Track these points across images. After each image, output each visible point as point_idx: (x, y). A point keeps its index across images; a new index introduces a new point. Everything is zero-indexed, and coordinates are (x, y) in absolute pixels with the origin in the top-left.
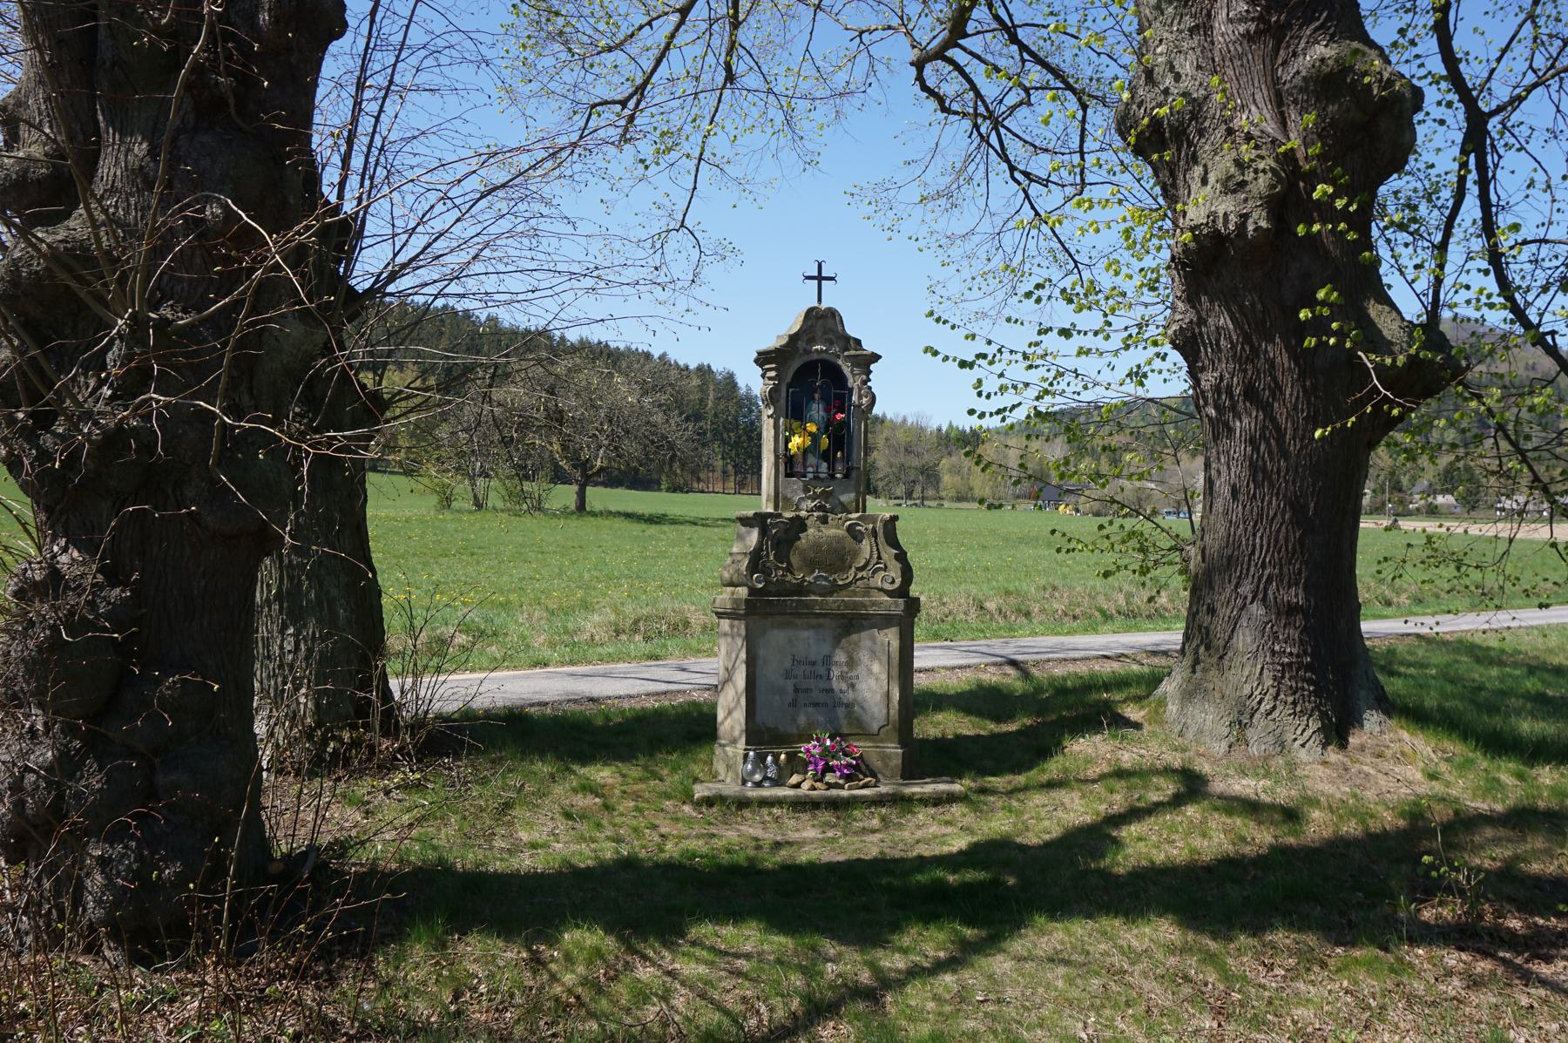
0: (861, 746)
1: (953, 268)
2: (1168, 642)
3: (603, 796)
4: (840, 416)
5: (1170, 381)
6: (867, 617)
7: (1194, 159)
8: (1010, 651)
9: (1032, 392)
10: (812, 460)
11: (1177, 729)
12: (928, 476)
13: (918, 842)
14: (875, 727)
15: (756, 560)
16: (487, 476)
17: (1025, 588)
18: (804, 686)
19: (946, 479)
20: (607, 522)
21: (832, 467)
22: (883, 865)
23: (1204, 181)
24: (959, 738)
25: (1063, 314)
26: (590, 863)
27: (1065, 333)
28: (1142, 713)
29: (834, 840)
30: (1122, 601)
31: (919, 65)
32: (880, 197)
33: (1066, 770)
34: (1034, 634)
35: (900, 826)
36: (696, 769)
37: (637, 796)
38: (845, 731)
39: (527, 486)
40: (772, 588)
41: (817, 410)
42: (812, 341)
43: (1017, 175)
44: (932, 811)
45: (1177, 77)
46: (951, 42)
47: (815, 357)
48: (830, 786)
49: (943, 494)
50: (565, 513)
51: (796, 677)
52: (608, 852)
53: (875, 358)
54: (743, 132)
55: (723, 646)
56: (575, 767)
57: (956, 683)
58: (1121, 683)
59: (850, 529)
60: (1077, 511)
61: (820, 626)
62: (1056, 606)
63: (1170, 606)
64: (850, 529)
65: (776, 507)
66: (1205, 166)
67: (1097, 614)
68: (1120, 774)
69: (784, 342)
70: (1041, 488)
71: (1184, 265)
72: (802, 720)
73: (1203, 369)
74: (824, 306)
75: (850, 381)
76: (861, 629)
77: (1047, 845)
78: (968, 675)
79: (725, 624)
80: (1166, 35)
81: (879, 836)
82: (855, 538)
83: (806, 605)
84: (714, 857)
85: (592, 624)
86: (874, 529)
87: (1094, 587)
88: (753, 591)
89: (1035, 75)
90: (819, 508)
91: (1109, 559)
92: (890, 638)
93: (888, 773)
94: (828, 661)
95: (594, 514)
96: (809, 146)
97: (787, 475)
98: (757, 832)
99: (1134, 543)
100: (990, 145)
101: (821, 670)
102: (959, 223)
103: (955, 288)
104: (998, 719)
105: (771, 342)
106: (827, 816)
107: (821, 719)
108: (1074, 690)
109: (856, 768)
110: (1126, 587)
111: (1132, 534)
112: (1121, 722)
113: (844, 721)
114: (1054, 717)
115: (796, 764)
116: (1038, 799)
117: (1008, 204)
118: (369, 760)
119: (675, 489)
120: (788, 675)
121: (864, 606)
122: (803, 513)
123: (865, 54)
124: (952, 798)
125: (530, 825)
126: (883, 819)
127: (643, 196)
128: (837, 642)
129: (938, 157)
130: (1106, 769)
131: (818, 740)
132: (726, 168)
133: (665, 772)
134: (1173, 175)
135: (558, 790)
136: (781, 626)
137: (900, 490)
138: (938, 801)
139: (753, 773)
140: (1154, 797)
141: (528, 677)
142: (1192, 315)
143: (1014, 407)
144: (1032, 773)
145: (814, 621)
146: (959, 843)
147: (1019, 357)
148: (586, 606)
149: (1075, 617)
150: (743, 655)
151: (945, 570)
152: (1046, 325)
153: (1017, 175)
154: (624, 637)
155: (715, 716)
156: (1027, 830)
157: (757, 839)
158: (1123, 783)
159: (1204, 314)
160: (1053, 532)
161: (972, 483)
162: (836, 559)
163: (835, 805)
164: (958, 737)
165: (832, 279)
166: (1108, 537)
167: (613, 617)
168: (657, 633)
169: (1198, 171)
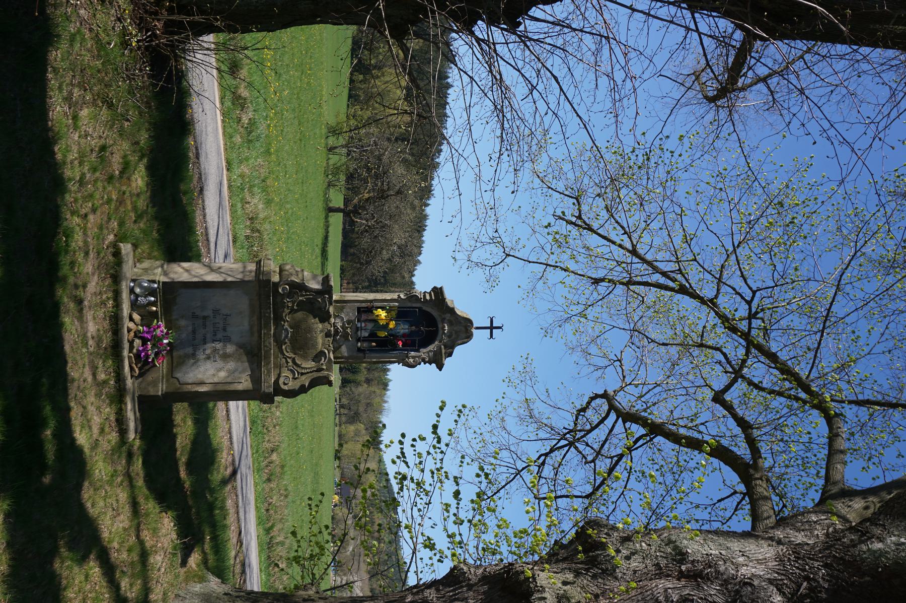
0: (162, 365)
1: (488, 421)
2: (251, 572)
3: (121, 177)
4: (400, 344)
5: (424, 568)
7: (577, 574)
8: (243, 469)
9: (417, 475)
10: (370, 326)
11: (181, 593)
12: (353, 417)
13: (84, 408)
14: (178, 375)
15: (300, 287)
16: (348, 155)
17: (286, 477)
19: (352, 428)
20: (322, 225)
21: (365, 340)
22: (60, 383)
23: (565, 583)
25: (469, 492)
26: (59, 156)
27: (457, 494)
28: (194, 566)
29: (86, 345)
30: (279, 539)
31: (605, 395)
32: (527, 375)
33: (147, 515)
34: (256, 484)
35: (98, 395)
36: (144, 247)
37: (121, 202)
38: (175, 354)
39: (343, 178)
41: (404, 329)
42: (451, 324)
43: (543, 458)
44: (113, 418)
45: (628, 558)
47: (440, 326)
48: (131, 343)
49: (343, 426)
50: (327, 200)
51: (214, 317)
52: (71, 173)
53: (440, 367)
54: (562, 290)
55: (238, 266)
56: (145, 160)
57: (218, 436)
58: (218, 547)
59: (322, 353)
60: (335, 506)
62: (275, 498)
64: (322, 353)
65: (336, 301)
66: (575, 582)
67: (270, 524)
68: (144, 555)
69: (449, 304)
70: (348, 485)
71: (508, 572)
73: (438, 590)
74: (474, 331)
75: (425, 350)
76: (250, 362)
77: (81, 507)
78: (225, 442)
79: (252, 267)
80: (653, 548)
81: (90, 379)
82: (316, 356)
84: (67, 252)
85: (256, 202)
86: (323, 369)
87: (287, 521)
88: (276, 285)
89: (603, 465)
91: (304, 532)
92: (244, 383)
94: (227, 340)
95: (327, 217)
96: (556, 331)
97: (359, 309)
98: (92, 287)
99: (317, 550)
100: (559, 440)
101: (220, 335)
102: (512, 423)
103: (474, 423)
104: (189, 464)
105: (449, 296)
106: (107, 340)
108: (212, 515)
109: (146, 362)
110: (288, 541)
111: (322, 548)
112: (186, 552)
113: (181, 353)
114: (191, 503)
115: (148, 318)
116: (123, 496)
117: (523, 453)
118: (146, 12)
119: (343, 270)
120: (216, 312)
122: (332, 320)
123: (608, 363)
124: (123, 432)
125: (95, 117)
126: (105, 382)
127: (523, 232)
128: (240, 346)
129: (552, 409)
130: (148, 545)
131: (167, 333)
132: (541, 282)
133: (142, 225)
134: (564, 560)
135: (126, 145)
137: (345, 401)
138: (121, 422)
139: (141, 287)
140: (124, 584)
141: (219, 154)
142: (474, 580)
143: (406, 463)
144: (145, 491)
145: (256, 329)
146: (82, 438)
147: (438, 466)
148: (268, 202)
149: (267, 510)
150: (229, 279)
151: (297, 427)
152: (461, 481)
153: (543, 458)
154: (248, 223)
155: (188, 260)
156: (96, 490)
157: (85, 286)
158: (136, 558)
159: (475, 588)
160: (322, 494)
162: (301, 343)
163: (115, 348)
164: (174, 437)
165: (491, 336)
166: (320, 532)
167: (261, 216)
169: (570, 577)
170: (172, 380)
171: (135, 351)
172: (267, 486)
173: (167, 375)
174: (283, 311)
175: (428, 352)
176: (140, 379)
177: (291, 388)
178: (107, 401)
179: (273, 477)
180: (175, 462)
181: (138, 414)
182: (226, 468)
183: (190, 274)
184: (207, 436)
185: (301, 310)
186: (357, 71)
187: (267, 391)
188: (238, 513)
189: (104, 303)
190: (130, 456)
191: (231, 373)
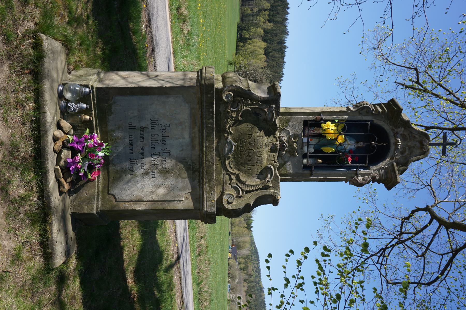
0: (98, 179)
6: (201, 184)
8: (184, 253)
14: (115, 191)
17: (209, 253)
18: (145, 135)
30: (205, 289)
31: (427, 209)
34: (192, 260)
38: (111, 168)
40: (222, 108)
41: (351, 145)
42: (404, 138)
46: (441, 222)
47: (392, 141)
48: (59, 154)
51: (153, 128)
60: (229, 258)
61: (193, 147)
63: (203, 306)
64: (267, 169)
65: (283, 114)
67: (200, 280)
72: (119, 134)
75: (375, 168)
76: (192, 179)
79: (194, 75)
82: (261, 173)
83: (209, 135)
86: (269, 187)
88: (220, 92)
90: (282, 146)
92: (185, 202)
93: (77, 202)
94: (166, 153)
97: (306, 122)
101: (158, 149)
104: (137, 272)
106: (26, 148)
107: (120, 149)
113: (116, 170)
120: (154, 122)
121: (210, 180)
122: (278, 134)
128: (181, 160)
145: (197, 142)
161: (236, 227)
162: (245, 158)
163: (39, 156)
164: (121, 249)
168: (184, 42)
171: (62, 163)
172: (198, 259)
173: (103, 192)
174: (227, 122)
175: (379, 170)
176: (75, 195)
177: (235, 208)
178: (27, 221)
180: (123, 272)
181: (71, 233)
182: (173, 256)
183: (127, 81)
184: (155, 243)
185: (246, 121)
186: (240, 41)
187: (209, 210)
188: (181, 284)
189: (19, 105)
190: (62, 279)
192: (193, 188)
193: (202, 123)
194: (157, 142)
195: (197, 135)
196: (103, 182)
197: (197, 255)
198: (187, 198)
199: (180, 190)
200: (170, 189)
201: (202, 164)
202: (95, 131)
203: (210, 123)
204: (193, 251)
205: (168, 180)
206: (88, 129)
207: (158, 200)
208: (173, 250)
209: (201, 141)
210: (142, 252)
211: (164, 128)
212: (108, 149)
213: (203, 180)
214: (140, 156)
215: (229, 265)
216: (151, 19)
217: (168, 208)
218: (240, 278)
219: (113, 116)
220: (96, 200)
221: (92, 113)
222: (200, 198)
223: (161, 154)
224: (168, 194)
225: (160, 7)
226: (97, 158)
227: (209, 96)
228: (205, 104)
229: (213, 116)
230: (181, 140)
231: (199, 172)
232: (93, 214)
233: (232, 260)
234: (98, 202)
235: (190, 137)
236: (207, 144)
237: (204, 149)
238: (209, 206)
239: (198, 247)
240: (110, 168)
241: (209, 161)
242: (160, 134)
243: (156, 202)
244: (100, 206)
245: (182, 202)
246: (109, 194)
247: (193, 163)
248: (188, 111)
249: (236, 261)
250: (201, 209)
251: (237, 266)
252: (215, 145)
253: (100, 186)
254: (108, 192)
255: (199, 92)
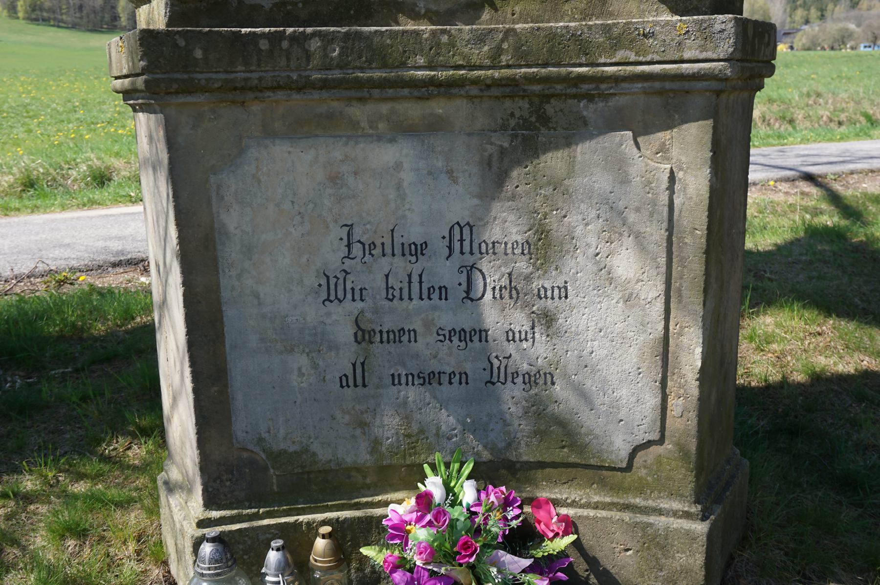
6: (594, 88)
8: (791, 162)
14: (619, 445)
24: (822, 384)
34: (805, 140)
38: (526, 454)
60: (792, 48)
61: (435, 126)
62: (821, 112)
67: (862, 119)
72: (389, 426)
76: (575, 131)
83: (379, 55)
92: (681, 157)
94: (464, 241)
101: (445, 272)
107: (447, 420)
120: (333, 289)
121: (582, 46)
128: (494, 178)
136: (299, 129)
145: (413, 110)
164: (818, 379)
170: (640, 472)
172: (801, 124)
179: (788, 116)
187: (726, 47)
191: (616, 223)
192: (613, 124)
193: (325, 85)
194: (415, 279)
195: (385, 108)
196: (580, 486)
197: (790, 129)
198: (663, 149)
199: (625, 181)
200: (618, 223)
201: (510, 83)
202: (378, 512)
203: (324, 48)
204: (780, 137)
205: (579, 231)
206: (365, 551)
207: (662, 278)
208: (787, 193)
209: (406, 91)
210: (829, 304)
211: (357, 249)
212: (447, 465)
213: (582, 78)
214: (476, 344)
215: (809, 49)
216: (129, 257)
217: (701, 232)
218: (847, 19)
219: (315, 447)
220: (652, 519)
221: (309, 524)
222: (661, 93)
223: (469, 260)
224: (638, 236)
225: (114, 231)
226: (481, 510)
227: (198, 54)
228: (240, 75)
229: (293, 38)
230: (407, 176)
231: (546, 98)
232: (710, 536)
233: (796, 40)
234: (660, 512)
235: (392, 140)
236: (421, 61)
237: (442, 74)
238: (703, 48)
239: (769, 125)
240: (525, 458)
241: (498, 51)
242: (385, 264)
243: (675, 285)
244: (676, 505)
245: (680, 175)
246: (629, 467)
247: (504, 128)
248: (280, 150)
249: (798, 30)
250: (714, 85)
251: (815, 28)
252: (426, 28)
253: (596, 498)
254: (620, 470)
255: (190, 99)
